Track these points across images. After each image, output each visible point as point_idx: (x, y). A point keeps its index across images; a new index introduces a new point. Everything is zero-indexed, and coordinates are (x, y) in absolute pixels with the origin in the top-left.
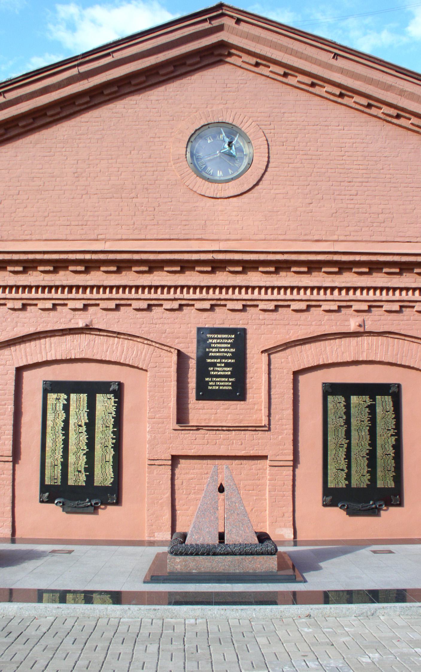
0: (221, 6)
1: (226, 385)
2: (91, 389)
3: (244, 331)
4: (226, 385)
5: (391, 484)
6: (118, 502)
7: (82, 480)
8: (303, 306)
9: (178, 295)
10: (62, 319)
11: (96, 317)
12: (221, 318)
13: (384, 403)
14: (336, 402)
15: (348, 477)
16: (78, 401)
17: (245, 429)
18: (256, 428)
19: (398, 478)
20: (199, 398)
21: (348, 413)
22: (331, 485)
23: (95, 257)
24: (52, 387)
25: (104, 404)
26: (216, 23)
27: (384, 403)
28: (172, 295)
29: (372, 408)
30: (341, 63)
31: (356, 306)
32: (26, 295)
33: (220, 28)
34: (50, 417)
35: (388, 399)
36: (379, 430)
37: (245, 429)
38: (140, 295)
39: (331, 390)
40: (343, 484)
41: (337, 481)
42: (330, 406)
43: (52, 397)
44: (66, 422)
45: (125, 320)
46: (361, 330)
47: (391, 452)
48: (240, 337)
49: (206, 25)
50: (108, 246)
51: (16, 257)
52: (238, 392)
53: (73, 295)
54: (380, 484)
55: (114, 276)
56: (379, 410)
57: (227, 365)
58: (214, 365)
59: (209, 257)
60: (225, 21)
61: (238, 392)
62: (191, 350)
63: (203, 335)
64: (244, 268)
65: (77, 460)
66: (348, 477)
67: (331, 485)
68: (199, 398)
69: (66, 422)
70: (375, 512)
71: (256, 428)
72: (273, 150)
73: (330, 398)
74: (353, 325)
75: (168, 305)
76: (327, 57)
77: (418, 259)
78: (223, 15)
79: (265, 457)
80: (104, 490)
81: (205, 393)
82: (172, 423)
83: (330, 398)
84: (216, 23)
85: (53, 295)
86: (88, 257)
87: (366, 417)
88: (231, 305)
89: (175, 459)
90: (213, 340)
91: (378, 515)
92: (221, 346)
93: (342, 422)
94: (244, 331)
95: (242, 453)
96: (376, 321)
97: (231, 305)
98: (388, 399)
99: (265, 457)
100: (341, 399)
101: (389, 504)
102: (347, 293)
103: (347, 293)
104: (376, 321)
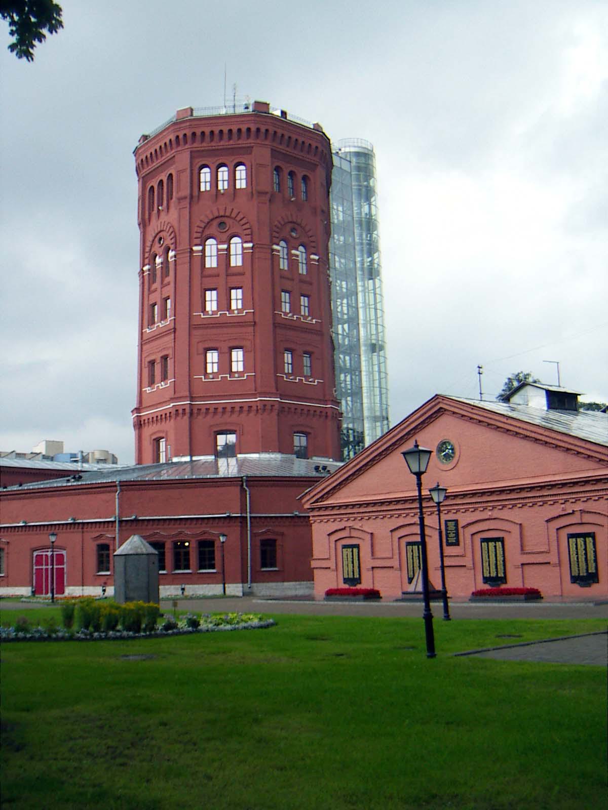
0: (436, 395)
3: (457, 520)
5: (503, 575)
7: (352, 577)
11: (496, 513)
13: (499, 544)
14: (572, 541)
15: (490, 573)
16: (580, 541)
20: (447, 545)
22: (573, 575)
24: (571, 536)
27: (589, 540)
29: (495, 547)
30: (474, 411)
33: (439, 403)
34: (408, 554)
35: (500, 543)
36: (498, 555)
41: (575, 573)
43: (408, 547)
44: (413, 555)
46: (361, 528)
47: (502, 563)
48: (456, 521)
49: (434, 403)
50: (557, 478)
52: (457, 543)
54: (499, 575)
56: (497, 548)
59: (462, 493)
65: (583, 565)
66: (490, 573)
67: (573, 575)
68: (447, 545)
69: (413, 555)
70: (589, 585)
73: (570, 540)
77: (607, 477)
81: (449, 544)
83: (570, 540)
87: (494, 550)
89: (522, 564)
90: (449, 523)
92: (451, 526)
94: (457, 520)
98: (500, 543)
100: (486, 544)
104: (496, 513)
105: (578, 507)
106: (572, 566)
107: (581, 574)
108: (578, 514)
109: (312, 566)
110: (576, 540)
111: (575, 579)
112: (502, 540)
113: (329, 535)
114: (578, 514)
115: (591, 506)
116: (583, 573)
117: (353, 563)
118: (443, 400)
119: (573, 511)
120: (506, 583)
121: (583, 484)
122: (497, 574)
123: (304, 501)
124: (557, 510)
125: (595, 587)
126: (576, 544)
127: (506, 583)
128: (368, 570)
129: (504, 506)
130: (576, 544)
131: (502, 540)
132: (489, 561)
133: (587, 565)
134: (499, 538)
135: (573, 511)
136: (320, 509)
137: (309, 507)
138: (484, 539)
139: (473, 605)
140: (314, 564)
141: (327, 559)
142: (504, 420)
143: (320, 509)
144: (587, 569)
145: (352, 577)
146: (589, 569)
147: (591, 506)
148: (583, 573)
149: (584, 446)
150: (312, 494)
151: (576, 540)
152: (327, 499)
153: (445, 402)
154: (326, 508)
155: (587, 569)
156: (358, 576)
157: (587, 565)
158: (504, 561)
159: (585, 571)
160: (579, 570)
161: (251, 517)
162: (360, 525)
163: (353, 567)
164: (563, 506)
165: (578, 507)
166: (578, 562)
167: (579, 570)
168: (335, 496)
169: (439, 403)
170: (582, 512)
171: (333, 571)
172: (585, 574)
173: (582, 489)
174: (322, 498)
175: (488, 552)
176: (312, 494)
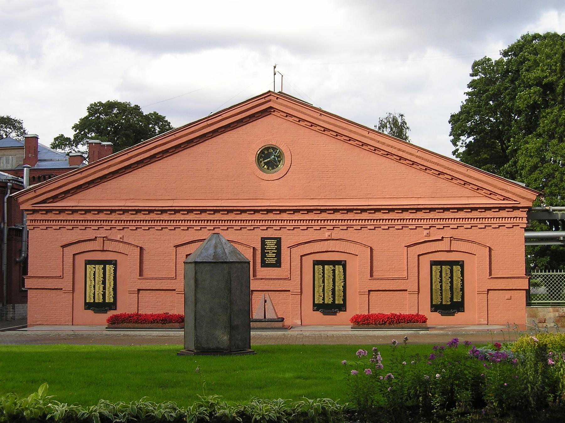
1: (273, 261)
2: (334, 263)
4: (273, 261)
6: (345, 311)
7: (101, 301)
8: (305, 227)
9: (253, 224)
10: (311, 235)
12: (270, 233)
13: (339, 269)
14: (319, 268)
15: (324, 299)
17: (281, 279)
18: (285, 279)
19: (344, 300)
21: (323, 273)
22: (316, 302)
23: (218, 208)
25: (456, 268)
26: (267, 99)
27: (456, 268)
28: (250, 224)
29: (334, 271)
30: (322, 118)
31: (328, 227)
32: (49, 223)
33: (270, 101)
35: (341, 267)
37: (281, 279)
38: (57, 223)
39: (434, 263)
40: (321, 302)
42: (316, 270)
45: (350, 234)
47: (342, 288)
48: (279, 241)
51: (184, 208)
52: (278, 264)
53: (54, 223)
55: (57, 216)
57: (273, 253)
58: (268, 253)
59: (266, 208)
60: (271, 97)
61: (278, 264)
62: (259, 247)
63: (263, 240)
64: (124, 212)
66: (324, 299)
67: (316, 302)
70: (335, 314)
71: (285, 279)
72: (293, 157)
73: (316, 266)
74: (326, 236)
75: (249, 228)
76: (317, 115)
78: (270, 95)
79: (406, 290)
80: (109, 304)
81: (264, 264)
82: (369, 277)
84: (267, 99)
85: (136, 224)
86: (215, 208)
88: (275, 228)
90: (268, 242)
91: (336, 315)
92: (271, 245)
93: (321, 276)
95: (280, 289)
96: (336, 234)
97: (275, 228)
98: (341, 267)
99: (406, 290)
101: (340, 310)
102: (324, 222)
103: (324, 222)
104: (336, 234)
105: (447, 233)
106: (434, 294)
107: (444, 303)
108: (447, 241)
109: (251, 289)
110: (441, 267)
111: (317, 307)
112: (343, 264)
113: (63, 247)
114: (447, 241)
115: (460, 233)
116: (339, 300)
117: (104, 283)
118: (277, 98)
119: (443, 237)
120: (116, 309)
121: (58, 212)
122: (334, 300)
123: (21, 199)
124: (422, 235)
125: (459, 315)
126: (441, 272)
127: (116, 309)
128: (361, 294)
129: (351, 226)
130: (441, 272)
131: (343, 264)
132: (324, 286)
133: (452, 294)
134: (112, 261)
135: (443, 237)
136: (48, 211)
137: (30, 208)
138: (89, 261)
139: (109, 333)
140: (28, 283)
141: (59, 277)
142: (365, 133)
143: (48, 211)
144: (452, 298)
145: (101, 301)
146: (454, 297)
147: (460, 233)
148: (446, 301)
149: (465, 172)
150: (39, 192)
151: (441, 267)
152: (63, 199)
153: (279, 100)
154: (61, 211)
155: (452, 298)
156: (112, 300)
157: (452, 294)
158: (344, 287)
159: (449, 300)
160: (442, 299)
161: (10, 230)
162: (121, 236)
163: (104, 288)
164: (427, 231)
165: (447, 233)
166: (441, 290)
167: (442, 299)
168: (74, 197)
169: (270, 101)
170: (452, 239)
171: (411, 293)
172: (449, 303)
173: (182, 217)
174: (55, 198)
175: (323, 276)
176: (39, 192)
